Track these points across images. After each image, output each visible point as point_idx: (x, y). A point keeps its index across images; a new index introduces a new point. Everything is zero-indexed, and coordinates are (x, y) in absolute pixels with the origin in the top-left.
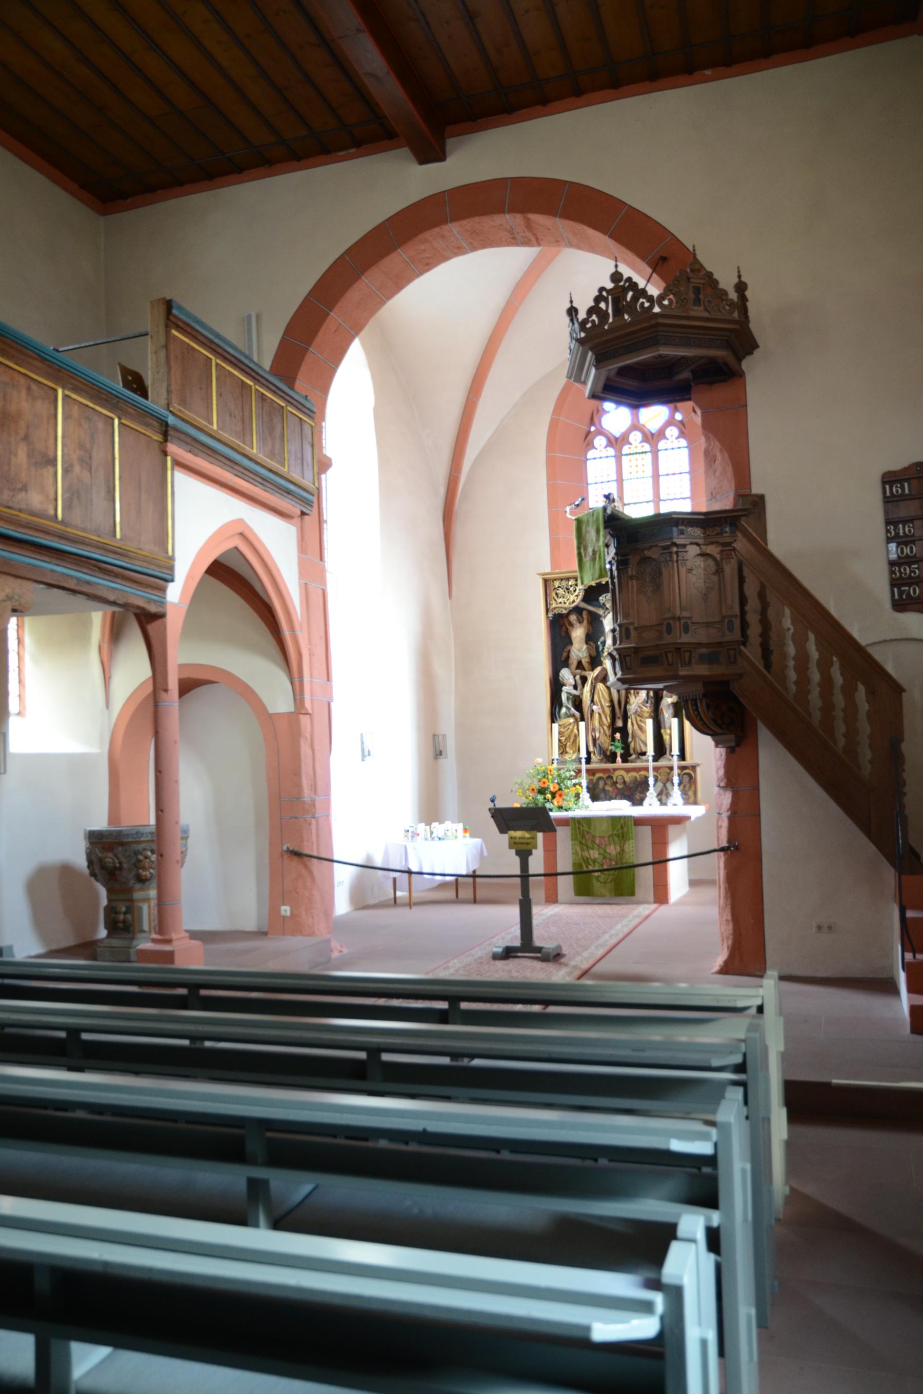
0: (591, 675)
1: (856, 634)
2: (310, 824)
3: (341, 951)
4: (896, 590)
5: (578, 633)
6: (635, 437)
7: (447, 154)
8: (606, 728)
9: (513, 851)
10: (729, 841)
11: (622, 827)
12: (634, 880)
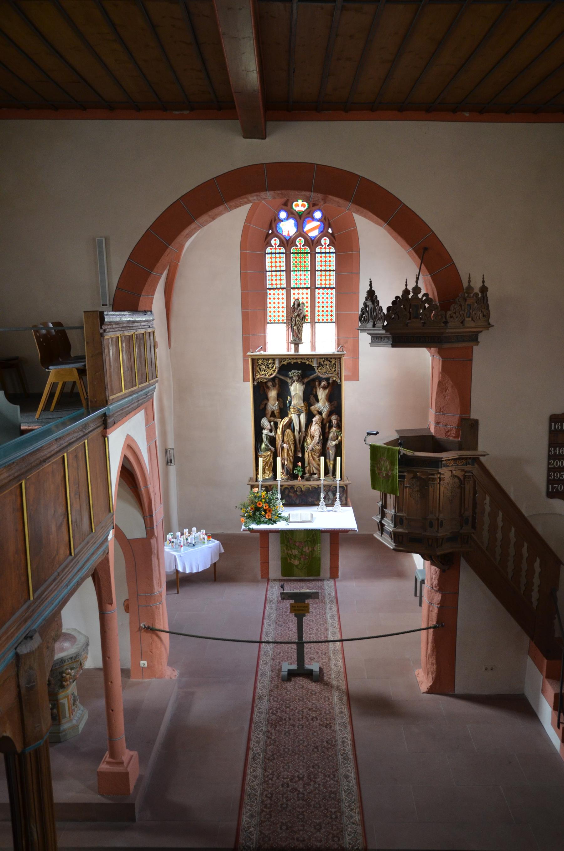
1: (523, 511)
5: (273, 394)
6: (300, 241)
8: (291, 458)
11: (313, 536)
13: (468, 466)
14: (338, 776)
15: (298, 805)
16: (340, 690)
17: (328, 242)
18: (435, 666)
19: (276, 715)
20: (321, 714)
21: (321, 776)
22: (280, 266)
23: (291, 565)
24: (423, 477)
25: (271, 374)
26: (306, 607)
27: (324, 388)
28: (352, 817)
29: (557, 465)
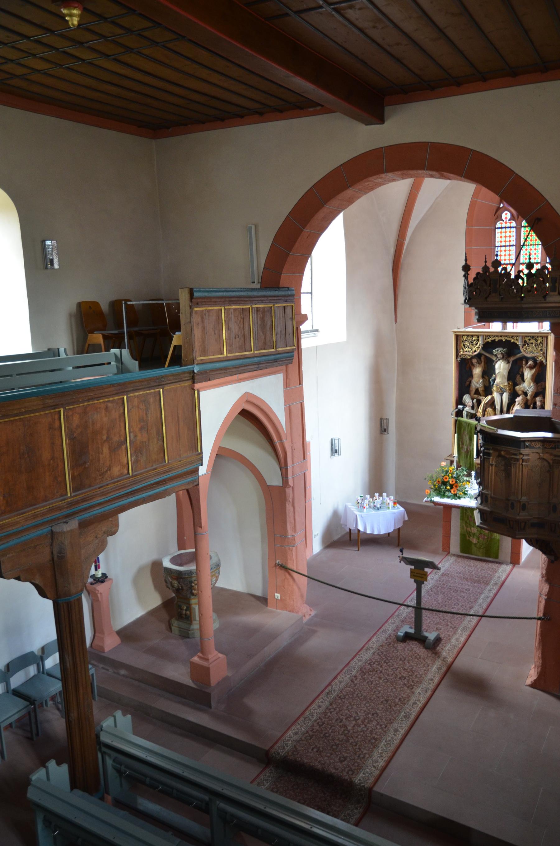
0: (486, 400)
2: (292, 550)
3: (310, 615)
5: (477, 371)
9: (413, 580)
10: (544, 615)
12: (498, 549)
13: (557, 450)
14: (388, 728)
15: (339, 738)
16: (445, 661)
17: (509, 216)
18: (540, 661)
21: (375, 723)
23: (470, 543)
24: (508, 456)
25: (475, 351)
26: (425, 575)
27: (531, 368)
28: (377, 762)
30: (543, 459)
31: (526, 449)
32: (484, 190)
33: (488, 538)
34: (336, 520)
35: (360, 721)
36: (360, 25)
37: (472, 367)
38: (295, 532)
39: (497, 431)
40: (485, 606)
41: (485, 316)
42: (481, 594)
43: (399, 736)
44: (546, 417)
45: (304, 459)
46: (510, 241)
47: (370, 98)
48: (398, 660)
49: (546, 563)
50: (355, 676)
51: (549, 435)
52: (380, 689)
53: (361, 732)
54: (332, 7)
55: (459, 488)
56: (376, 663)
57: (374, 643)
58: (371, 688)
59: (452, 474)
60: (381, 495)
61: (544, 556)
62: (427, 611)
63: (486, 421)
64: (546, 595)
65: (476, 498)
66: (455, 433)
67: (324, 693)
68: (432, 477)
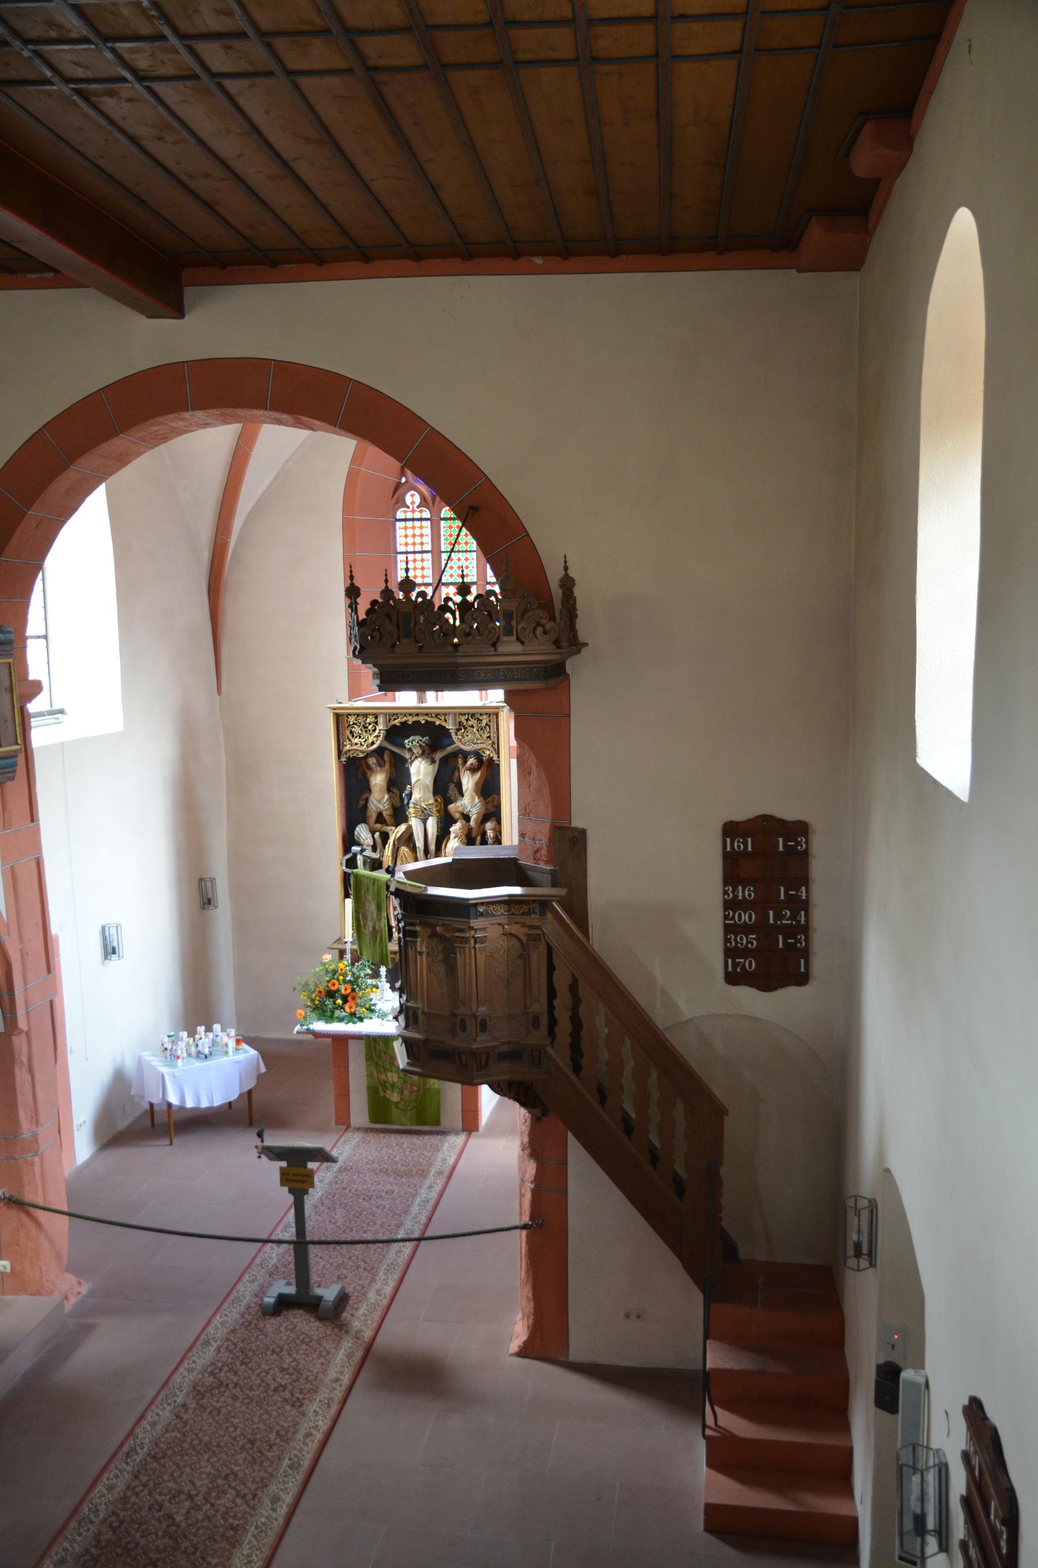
2: (32, 1165)
4: (730, 961)
5: (378, 780)
7: (186, 310)
9: (286, 1189)
10: (532, 1218)
12: (439, 1108)
13: (533, 916)
15: (157, 1547)
16: (358, 1339)
17: (417, 499)
18: (531, 1305)
19: (215, 1377)
20: (298, 1380)
22: (422, 544)
23: (386, 1101)
24: (448, 935)
25: (373, 743)
27: (473, 770)
29: (740, 919)
30: (511, 934)
31: (480, 919)
32: (373, 450)
33: (419, 1089)
34: (120, 1089)
35: (199, 1500)
36: (133, 130)
37: (368, 772)
38: (37, 1126)
39: (426, 889)
40: (423, 1219)
41: (389, 682)
42: (414, 1196)
43: (283, 1510)
44: (510, 859)
45: (49, 972)
46: (422, 544)
47: (159, 269)
48: (269, 1353)
49: (529, 1121)
50: (184, 1406)
51: (517, 890)
52: (236, 1421)
53: (203, 1520)
54: (72, 86)
55: (358, 1001)
56: (226, 1369)
57: (217, 1328)
58: (217, 1422)
59: (345, 975)
60: (209, 1029)
61: (523, 1111)
62: (318, 1246)
63: (405, 873)
64: (532, 1182)
65: (396, 1018)
66: (347, 895)
67: (121, 1455)
68: (307, 984)
